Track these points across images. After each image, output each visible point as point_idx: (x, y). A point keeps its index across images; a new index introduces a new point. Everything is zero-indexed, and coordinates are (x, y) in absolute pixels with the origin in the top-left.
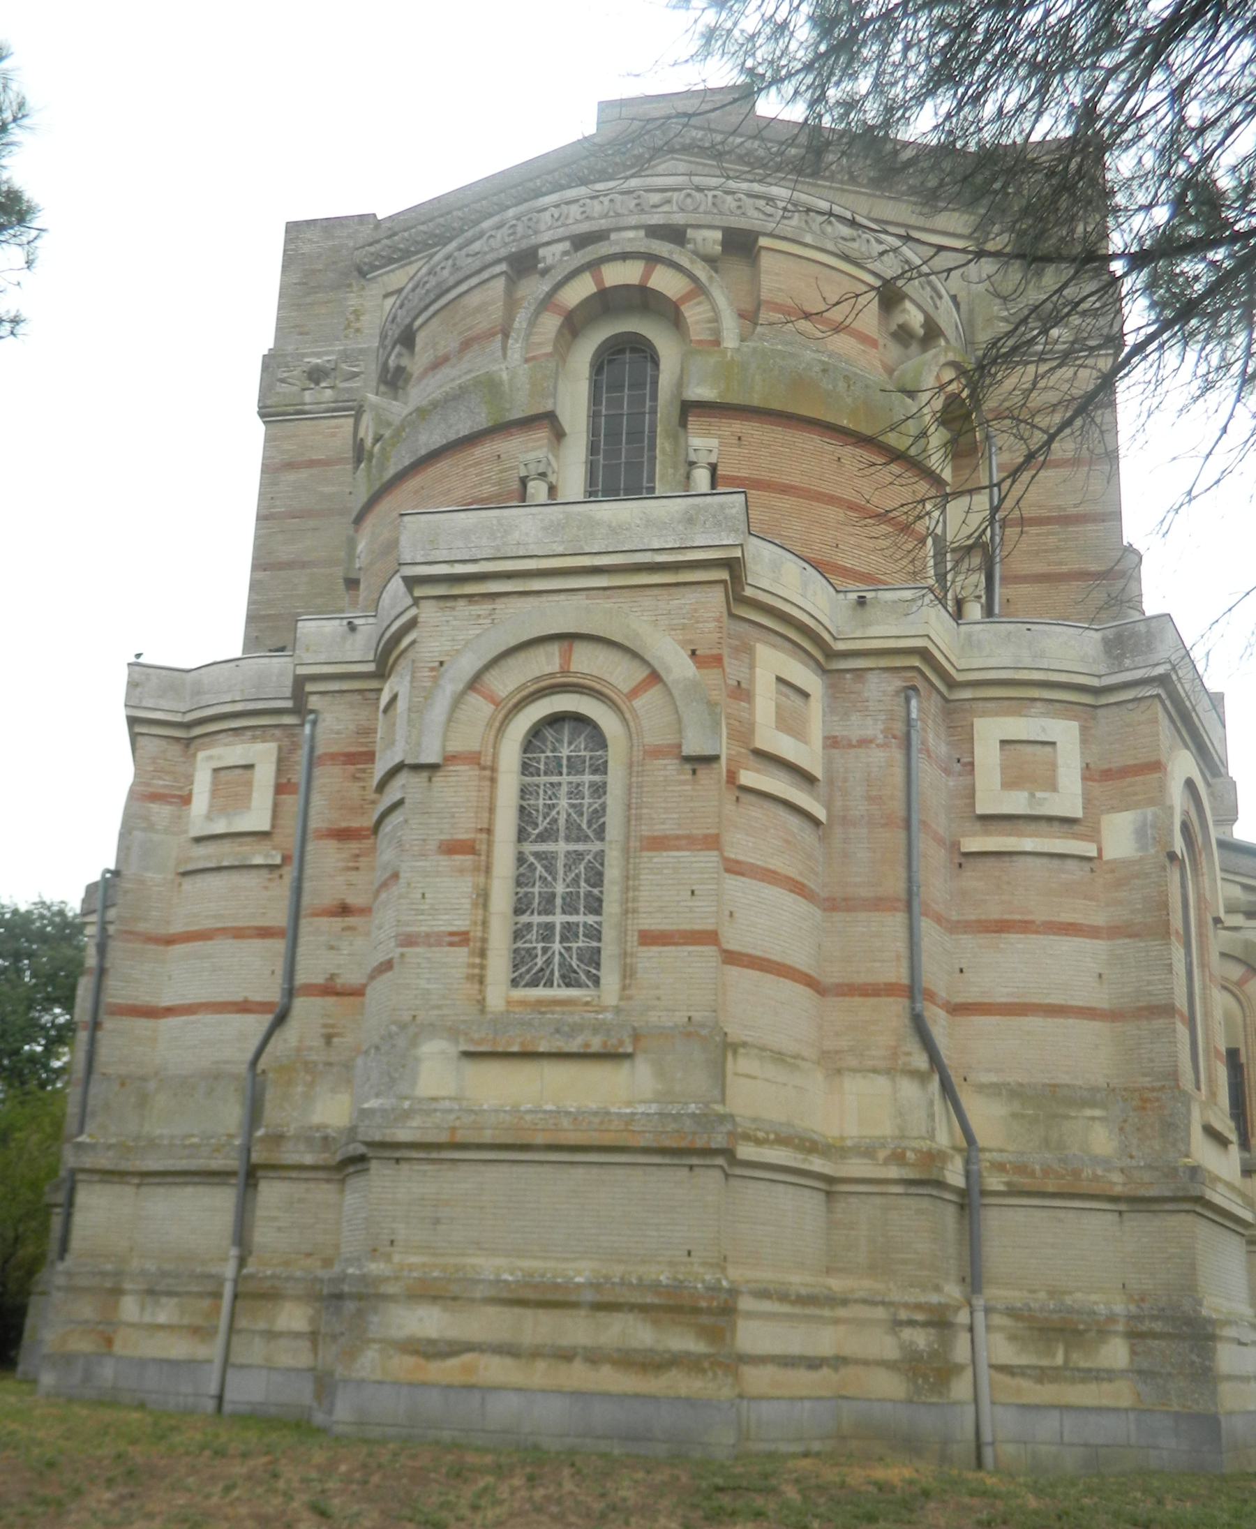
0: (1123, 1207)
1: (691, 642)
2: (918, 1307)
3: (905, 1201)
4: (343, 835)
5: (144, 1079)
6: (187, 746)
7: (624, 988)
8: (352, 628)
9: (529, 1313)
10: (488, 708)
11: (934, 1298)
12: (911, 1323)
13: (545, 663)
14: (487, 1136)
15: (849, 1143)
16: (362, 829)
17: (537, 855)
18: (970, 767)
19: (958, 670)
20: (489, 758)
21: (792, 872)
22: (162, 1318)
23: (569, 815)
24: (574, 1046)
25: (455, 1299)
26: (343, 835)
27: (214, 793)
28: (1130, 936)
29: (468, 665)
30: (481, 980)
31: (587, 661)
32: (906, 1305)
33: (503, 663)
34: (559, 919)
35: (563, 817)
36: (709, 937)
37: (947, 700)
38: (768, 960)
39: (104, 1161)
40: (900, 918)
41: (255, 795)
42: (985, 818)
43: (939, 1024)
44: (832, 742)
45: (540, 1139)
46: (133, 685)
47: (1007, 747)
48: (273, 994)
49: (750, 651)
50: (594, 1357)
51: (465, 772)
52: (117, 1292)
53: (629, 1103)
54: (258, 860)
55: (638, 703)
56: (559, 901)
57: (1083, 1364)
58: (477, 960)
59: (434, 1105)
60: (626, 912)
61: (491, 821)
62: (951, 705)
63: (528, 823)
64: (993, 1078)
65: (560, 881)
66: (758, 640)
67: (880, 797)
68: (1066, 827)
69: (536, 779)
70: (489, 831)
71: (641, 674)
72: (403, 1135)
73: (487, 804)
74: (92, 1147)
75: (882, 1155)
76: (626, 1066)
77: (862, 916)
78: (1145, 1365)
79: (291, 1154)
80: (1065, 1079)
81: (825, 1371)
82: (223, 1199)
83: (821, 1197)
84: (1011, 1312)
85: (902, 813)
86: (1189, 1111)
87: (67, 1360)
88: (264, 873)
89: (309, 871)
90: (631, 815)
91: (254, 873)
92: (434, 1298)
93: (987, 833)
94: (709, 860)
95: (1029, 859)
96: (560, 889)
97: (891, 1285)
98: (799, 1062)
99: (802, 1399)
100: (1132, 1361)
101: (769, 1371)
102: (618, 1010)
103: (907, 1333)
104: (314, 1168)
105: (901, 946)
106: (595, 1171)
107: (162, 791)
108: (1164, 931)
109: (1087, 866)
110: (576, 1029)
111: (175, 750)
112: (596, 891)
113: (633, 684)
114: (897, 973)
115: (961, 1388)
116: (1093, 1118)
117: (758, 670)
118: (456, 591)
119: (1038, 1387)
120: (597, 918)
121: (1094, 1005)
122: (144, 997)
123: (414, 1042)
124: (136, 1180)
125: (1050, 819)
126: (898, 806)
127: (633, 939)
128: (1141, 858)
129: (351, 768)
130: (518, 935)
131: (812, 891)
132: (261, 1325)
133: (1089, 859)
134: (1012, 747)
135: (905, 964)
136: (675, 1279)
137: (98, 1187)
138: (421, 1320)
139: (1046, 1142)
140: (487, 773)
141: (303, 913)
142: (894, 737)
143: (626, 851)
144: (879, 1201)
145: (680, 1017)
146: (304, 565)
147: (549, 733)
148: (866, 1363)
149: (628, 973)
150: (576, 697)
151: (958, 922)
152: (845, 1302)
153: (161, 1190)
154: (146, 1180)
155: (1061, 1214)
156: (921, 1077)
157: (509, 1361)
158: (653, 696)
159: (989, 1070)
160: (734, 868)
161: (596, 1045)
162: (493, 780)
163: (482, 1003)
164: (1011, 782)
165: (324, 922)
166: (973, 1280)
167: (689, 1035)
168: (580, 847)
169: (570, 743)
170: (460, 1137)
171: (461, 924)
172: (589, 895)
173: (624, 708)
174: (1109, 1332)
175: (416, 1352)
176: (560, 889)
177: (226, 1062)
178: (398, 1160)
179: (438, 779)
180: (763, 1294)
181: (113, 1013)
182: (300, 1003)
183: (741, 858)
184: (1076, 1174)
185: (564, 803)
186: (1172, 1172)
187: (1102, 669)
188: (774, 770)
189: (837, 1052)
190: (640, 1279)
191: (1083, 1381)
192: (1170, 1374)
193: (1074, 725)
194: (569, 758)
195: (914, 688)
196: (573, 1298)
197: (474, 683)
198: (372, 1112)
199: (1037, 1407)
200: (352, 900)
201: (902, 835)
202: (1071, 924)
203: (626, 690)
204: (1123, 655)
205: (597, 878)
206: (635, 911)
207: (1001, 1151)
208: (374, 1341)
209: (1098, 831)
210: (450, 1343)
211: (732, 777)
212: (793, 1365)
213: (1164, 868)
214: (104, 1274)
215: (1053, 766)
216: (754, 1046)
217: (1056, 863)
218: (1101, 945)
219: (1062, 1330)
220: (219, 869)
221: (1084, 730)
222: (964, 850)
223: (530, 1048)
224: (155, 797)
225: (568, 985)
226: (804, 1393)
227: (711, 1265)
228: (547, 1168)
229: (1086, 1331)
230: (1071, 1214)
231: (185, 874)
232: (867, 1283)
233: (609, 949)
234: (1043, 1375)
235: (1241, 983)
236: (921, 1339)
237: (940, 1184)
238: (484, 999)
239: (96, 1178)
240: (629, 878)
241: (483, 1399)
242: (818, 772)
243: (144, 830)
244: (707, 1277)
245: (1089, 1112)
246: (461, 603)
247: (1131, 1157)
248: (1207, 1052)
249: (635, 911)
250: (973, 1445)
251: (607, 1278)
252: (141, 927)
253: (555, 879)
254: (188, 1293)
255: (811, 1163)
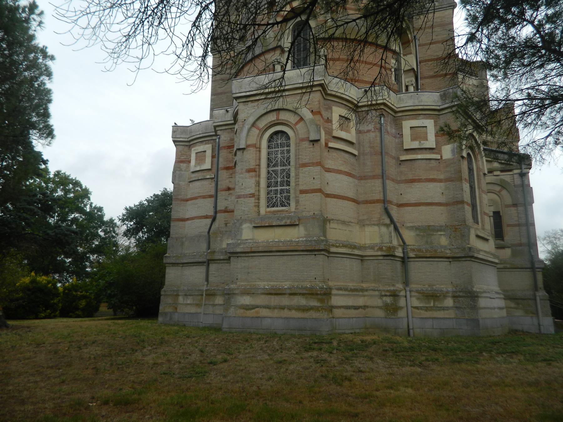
0: (451, 260)
1: (311, 108)
2: (388, 291)
3: (384, 261)
4: (228, 168)
5: (182, 238)
6: (190, 147)
7: (296, 206)
8: (227, 111)
9: (273, 297)
10: (258, 131)
11: (392, 288)
12: (386, 296)
13: (272, 117)
14: (260, 249)
15: (367, 245)
16: (232, 167)
17: (273, 171)
18: (402, 135)
19: (397, 108)
20: (258, 145)
21: (346, 170)
22: (189, 302)
23: (281, 159)
24: (283, 223)
25: (253, 294)
26: (228, 168)
27: (196, 159)
28: (451, 181)
29: (251, 120)
30: (258, 206)
31: (284, 116)
32: (384, 291)
33: (261, 118)
34: (279, 188)
35: (279, 161)
36: (320, 191)
37: (395, 117)
38: (339, 195)
39: (172, 260)
40: (380, 181)
41: (207, 159)
42: (407, 150)
43: (394, 211)
44: (359, 132)
45: (274, 249)
46: (174, 132)
47: (412, 129)
48: (211, 213)
49: (331, 109)
50: (290, 308)
51: (252, 150)
52: (178, 295)
53: (298, 238)
54: (208, 177)
55: (297, 127)
56: (279, 183)
57: (439, 306)
58: (257, 201)
59: (247, 241)
60: (296, 185)
61: (260, 162)
62: (396, 118)
63: (270, 162)
64: (411, 225)
65: (279, 178)
66: (333, 105)
67: (373, 147)
68: (431, 151)
69: (272, 150)
70: (259, 165)
71: (298, 118)
72: (238, 250)
73: (258, 158)
74: (169, 257)
75: (376, 248)
76: (297, 228)
77: (369, 181)
78: (458, 305)
79: (217, 256)
80: (432, 224)
81: (360, 310)
82: (203, 269)
83: (360, 261)
84: (417, 291)
85: (380, 151)
86: (469, 231)
87: (166, 314)
88: (210, 180)
89: (219, 179)
90: (297, 158)
91: (207, 180)
92: (248, 294)
93: (407, 154)
94: (318, 168)
95: (420, 161)
96: (279, 180)
97: (380, 285)
98: (350, 223)
99: (353, 318)
100: (454, 304)
101: (342, 310)
102: (295, 212)
103: (384, 298)
104: (223, 260)
105: (381, 189)
106: (290, 257)
107: (184, 160)
108: (460, 179)
109: (438, 162)
110: (283, 218)
111: (186, 148)
112: (289, 180)
113: (296, 121)
114: (380, 196)
115: (402, 314)
116: (441, 235)
117: (333, 114)
118: (248, 100)
119: (426, 312)
120: (289, 187)
121: (442, 202)
122: (181, 216)
123: (241, 224)
124: (181, 265)
125: (426, 149)
126: (378, 149)
127: (298, 192)
128: (453, 158)
129: (229, 150)
130: (268, 193)
131: (354, 175)
132: (211, 303)
133: (439, 159)
134: (414, 129)
135: (382, 193)
136: (311, 286)
137: (172, 267)
138: (244, 300)
139: (427, 242)
140: (258, 149)
141: (218, 190)
142: (377, 129)
143: (296, 168)
144: (376, 261)
145: (311, 213)
146: (225, 93)
147: (275, 137)
148: (373, 307)
149: (297, 202)
150: (281, 126)
151: (400, 180)
152: (367, 290)
153: (187, 268)
154: (184, 265)
155: (432, 263)
156: (387, 226)
157: (268, 310)
158: (301, 124)
159: (409, 223)
160: (328, 170)
161: (288, 222)
162: (260, 151)
163: (259, 213)
164: (413, 139)
165: (224, 193)
166: (406, 283)
167: (314, 218)
168: (284, 168)
169: (280, 139)
170: (253, 250)
171: (252, 191)
172: (287, 181)
173: (294, 128)
174: (447, 296)
175: (244, 309)
176: (279, 180)
177: (202, 232)
178: (238, 257)
179: (245, 152)
180: (340, 289)
181: (173, 221)
182: (218, 215)
183: (330, 167)
184: (436, 251)
185: (279, 156)
186: (464, 249)
187: (440, 104)
188: (339, 141)
189: (363, 220)
190: (302, 286)
191: (439, 310)
192: (465, 308)
193: (432, 121)
194: (280, 143)
195: (383, 114)
196: (284, 292)
197: (254, 125)
198: (230, 244)
199: (426, 318)
200: (231, 186)
201: (380, 157)
202: (433, 179)
203: (294, 123)
204: (446, 99)
205: (288, 176)
206: (298, 185)
207: (414, 245)
208: (233, 306)
209: (441, 151)
210: (252, 305)
211: (326, 145)
212: (350, 308)
213: (460, 161)
214: (174, 291)
215: (426, 133)
216: (336, 220)
217: (428, 161)
218: (442, 184)
219: (432, 296)
220: (198, 180)
221: (435, 122)
222: (400, 159)
223: (271, 225)
224: (182, 162)
225: (282, 206)
226: (354, 316)
227: (321, 282)
228: (277, 257)
229: (440, 296)
230: (435, 263)
231: (190, 182)
232: (373, 285)
233: (292, 195)
234: (427, 309)
235: (499, 192)
236: (388, 300)
237: (394, 256)
238: (259, 212)
239: (171, 265)
240: (297, 175)
241: (261, 320)
242: (354, 141)
243: (179, 171)
244: (320, 285)
245: (439, 233)
246: (249, 103)
247: (453, 245)
248: (481, 213)
249: (298, 185)
250: (407, 330)
251: (293, 286)
252: (180, 197)
253: (278, 177)
254: (195, 295)
255: (354, 252)
